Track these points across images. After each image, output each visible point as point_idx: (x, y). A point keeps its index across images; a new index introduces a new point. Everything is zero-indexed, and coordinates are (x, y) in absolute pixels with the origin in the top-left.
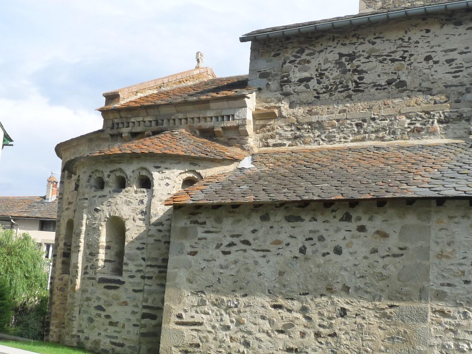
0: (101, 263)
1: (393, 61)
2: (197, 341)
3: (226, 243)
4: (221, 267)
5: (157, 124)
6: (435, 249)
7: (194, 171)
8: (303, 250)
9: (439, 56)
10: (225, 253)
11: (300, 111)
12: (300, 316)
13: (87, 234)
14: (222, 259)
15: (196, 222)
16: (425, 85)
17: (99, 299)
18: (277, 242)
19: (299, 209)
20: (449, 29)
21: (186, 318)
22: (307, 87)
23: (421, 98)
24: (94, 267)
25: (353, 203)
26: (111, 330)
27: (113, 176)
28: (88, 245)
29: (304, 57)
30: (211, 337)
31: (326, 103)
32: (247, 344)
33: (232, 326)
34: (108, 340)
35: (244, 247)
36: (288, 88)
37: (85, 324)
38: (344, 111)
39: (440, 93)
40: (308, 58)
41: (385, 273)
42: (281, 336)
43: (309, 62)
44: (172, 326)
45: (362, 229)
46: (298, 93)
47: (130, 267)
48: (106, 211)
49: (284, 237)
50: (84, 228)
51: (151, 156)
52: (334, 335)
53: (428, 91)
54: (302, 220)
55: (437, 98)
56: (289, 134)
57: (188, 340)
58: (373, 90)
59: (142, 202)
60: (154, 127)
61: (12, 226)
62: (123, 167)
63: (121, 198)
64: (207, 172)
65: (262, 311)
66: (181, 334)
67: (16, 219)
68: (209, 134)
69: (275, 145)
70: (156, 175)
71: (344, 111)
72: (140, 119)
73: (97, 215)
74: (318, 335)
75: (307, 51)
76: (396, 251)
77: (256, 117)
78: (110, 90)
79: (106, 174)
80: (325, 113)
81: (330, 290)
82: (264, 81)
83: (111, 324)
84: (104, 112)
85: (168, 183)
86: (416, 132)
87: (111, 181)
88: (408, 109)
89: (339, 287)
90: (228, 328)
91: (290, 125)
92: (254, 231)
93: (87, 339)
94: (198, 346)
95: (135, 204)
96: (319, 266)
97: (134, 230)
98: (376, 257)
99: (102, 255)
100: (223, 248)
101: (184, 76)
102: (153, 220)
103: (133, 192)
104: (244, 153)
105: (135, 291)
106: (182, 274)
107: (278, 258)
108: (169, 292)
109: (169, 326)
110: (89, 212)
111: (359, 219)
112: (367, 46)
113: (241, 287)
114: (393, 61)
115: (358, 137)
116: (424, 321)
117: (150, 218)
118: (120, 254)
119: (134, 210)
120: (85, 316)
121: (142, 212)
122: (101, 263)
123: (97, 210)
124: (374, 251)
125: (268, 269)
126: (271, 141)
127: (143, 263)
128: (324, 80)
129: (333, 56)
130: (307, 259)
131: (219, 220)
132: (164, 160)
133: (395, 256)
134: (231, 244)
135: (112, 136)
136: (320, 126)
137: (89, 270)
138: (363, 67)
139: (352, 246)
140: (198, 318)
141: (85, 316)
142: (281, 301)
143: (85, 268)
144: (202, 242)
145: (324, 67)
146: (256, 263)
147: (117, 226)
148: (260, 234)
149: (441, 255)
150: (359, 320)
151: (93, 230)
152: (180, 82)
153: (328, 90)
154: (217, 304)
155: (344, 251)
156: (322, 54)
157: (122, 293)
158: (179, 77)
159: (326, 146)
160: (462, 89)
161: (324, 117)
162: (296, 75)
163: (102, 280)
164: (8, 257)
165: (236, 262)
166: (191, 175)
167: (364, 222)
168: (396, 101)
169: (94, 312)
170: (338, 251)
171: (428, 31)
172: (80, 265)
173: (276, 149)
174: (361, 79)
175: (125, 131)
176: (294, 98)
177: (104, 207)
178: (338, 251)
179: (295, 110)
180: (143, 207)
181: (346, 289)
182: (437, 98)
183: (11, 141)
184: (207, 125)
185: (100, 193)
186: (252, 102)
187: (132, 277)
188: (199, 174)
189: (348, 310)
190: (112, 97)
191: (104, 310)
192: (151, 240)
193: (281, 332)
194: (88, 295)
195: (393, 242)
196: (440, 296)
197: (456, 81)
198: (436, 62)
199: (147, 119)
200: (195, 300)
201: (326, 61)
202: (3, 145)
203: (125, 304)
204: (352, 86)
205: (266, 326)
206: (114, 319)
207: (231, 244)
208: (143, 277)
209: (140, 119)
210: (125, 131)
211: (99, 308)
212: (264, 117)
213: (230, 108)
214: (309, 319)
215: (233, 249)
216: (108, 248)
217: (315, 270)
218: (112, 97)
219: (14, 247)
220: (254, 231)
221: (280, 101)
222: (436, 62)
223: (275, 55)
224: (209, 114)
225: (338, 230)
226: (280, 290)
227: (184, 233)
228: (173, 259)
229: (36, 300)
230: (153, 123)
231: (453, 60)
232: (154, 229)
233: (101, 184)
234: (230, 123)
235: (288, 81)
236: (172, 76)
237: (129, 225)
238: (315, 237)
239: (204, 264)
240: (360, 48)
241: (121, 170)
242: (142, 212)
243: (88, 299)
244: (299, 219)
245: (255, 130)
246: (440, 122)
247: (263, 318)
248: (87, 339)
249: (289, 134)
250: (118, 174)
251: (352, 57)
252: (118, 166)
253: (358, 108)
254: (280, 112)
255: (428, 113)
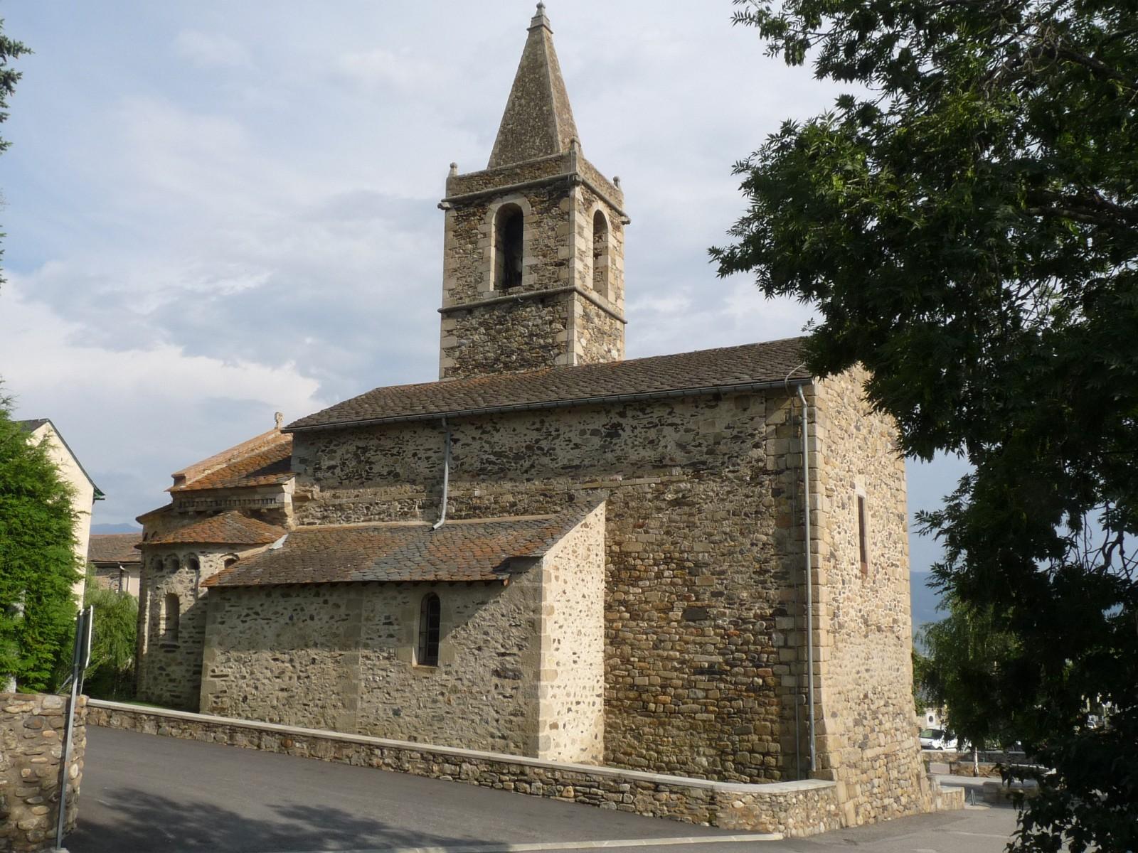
0: (162, 632)
1: (392, 455)
2: (225, 688)
3: (244, 614)
4: (241, 632)
5: (217, 504)
6: (365, 614)
7: (232, 554)
8: (291, 618)
9: (422, 454)
10: (244, 622)
11: (328, 494)
12: (289, 665)
13: (151, 608)
14: (241, 627)
15: (224, 599)
16: (412, 476)
17: (160, 661)
18: (276, 613)
19: (288, 590)
20: (427, 432)
21: (218, 672)
22: (333, 473)
23: (408, 487)
24: (157, 635)
25: (319, 585)
26: (171, 685)
27: (169, 560)
28: (152, 618)
29: (332, 447)
30: (234, 684)
31: (346, 488)
32: (256, 688)
33: (247, 676)
34: (168, 694)
35: (255, 616)
36: (319, 475)
37: (151, 682)
38: (358, 496)
39: (421, 483)
40: (335, 448)
41: (337, 632)
42: (278, 680)
43: (335, 452)
44: (209, 679)
45: (326, 602)
46: (326, 479)
47: (185, 634)
48: (165, 589)
49: (280, 609)
50: (148, 603)
51: (196, 544)
52: (308, 677)
53: (413, 482)
54: (290, 596)
55: (418, 488)
56: (319, 515)
57: (219, 688)
58: (378, 479)
59: (191, 581)
60: (215, 508)
61: (122, 574)
62: (177, 552)
63: (175, 578)
64: (242, 555)
65: (265, 663)
66: (214, 684)
67: (125, 564)
68: (257, 514)
69: (309, 524)
70: (202, 559)
71: (358, 496)
72: (203, 499)
73: (158, 592)
74: (299, 678)
75: (335, 443)
76: (344, 617)
77: (295, 499)
78: (177, 471)
79: (164, 558)
80: (346, 496)
81: (307, 646)
82: (303, 466)
83: (171, 680)
84: (173, 493)
85: (212, 565)
86: (404, 515)
87: (168, 563)
88: (400, 496)
89: (312, 643)
90: (244, 677)
91: (320, 507)
92: (262, 605)
93: (153, 694)
94: (225, 692)
95: (187, 583)
96: (300, 629)
97: (186, 604)
98: (333, 621)
99: (163, 625)
100: (242, 618)
101: (257, 443)
102: (200, 595)
103: (185, 573)
104: (285, 531)
105: (188, 653)
106: (216, 639)
107: (275, 625)
108: (206, 651)
109: (207, 678)
110: (152, 590)
111: (324, 595)
112: (375, 442)
113: (253, 646)
114: (392, 455)
115: (367, 518)
116: (357, 663)
117: (198, 594)
118: (177, 623)
119: (185, 588)
120: (151, 676)
121: (192, 589)
122: (162, 632)
123: (158, 588)
124: (332, 618)
125: (270, 632)
126: (306, 520)
127: (194, 630)
128: (346, 468)
129: (352, 448)
130: (293, 625)
131: (239, 597)
132: (208, 547)
133: (344, 620)
134: (247, 615)
135: (180, 513)
136: (340, 508)
137: (154, 638)
138: (373, 459)
139: (320, 616)
140: (226, 671)
141: (151, 676)
142: (278, 655)
143: (150, 637)
144: (229, 614)
145: (346, 457)
146: (263, 628)
147: (173, 600)
148: (265, 607)
149: (368, 619)
150: (322, 666)
151: (155, 605)
152: (253, 450)
153: (349, 478)
154: (238, 660)
155: (316, 618)
156: (345, 446)
157: (178, 656)
158: (251, 446)
159: (345, 525)
160: (434, 482)
161: (344, 500)
162: (326, 463)
163: (163, 646)
164: (107, 620)
165: (250, 628)
166: (231, 557)
167: (327, 597)
168: (392, 489)
169: (157, 672)
170: (312, 618)
171: (415, 432)
172: (146, 634)
173: (309, 527)
174: (371, 469)
175: (191, 509)
176: (324, 483)
177: (164, 586)
178: (312, 618)
179: (324, 494)
180: (192, 585)
181: (316, 645)
182: (418, 488)
183: (102, 494)
184: (256, 506)
185: (160, 574)
186: (290, 487)
187: (186, 642)
188: (237, 556)
189: (913, 656)
190: (179, 479)
191: (164, 670)
192: (199, 612)
193: (277, 677)
194: (153, 658)
195: (343, 611)
196: (366, 646)
197: (431, 475)
198: (419, 459)
199: (209, 500)
200: (223, 658)
201: (348, 452)
202: (94, 500)
203: (181, 664)
204: (364, 474)
205: (269, 674)
206: (173, 677)
207: (247, 615)
208: (194, 642)
209: (203, 499)
210: (191, 509)
211: (161, 668)
212: (299, 499)
213: (272, 493)
214: (294, 667)
215: (248, 619)
216: (167, 619)
217: (298, 632)
218: (179, 479)
219: (113, 608)
220: (262, 605)
221: (312, 485)
222: (419, 459)
223: (313, 444)
224: (257, 497)
225: (312, 603)
226: (277, 646)
227: (217, 607)
228: (209, 628)
229: (766, 710)
230: (214, 504)
231: (430, 457)
232: (200, 603)
233: (161, 567)
234: (272, 506)
235: (319, 469)
236: (242, 445)
237: (182, 600)
238: (298, 608)
239: (230, 631)
240: (371, 443)
241: (175, 555)
242: (192, 589)
243: (153, 662)
244: (289, 595)
245: (294, 510)
246: (419, 507)
247: (267, 668)
248: (153, 694)
249: (319, 515)
250: (174, 558)
251: (365, 450)
252: (173, 551)
253: (368, 493)
254: (312, 495)
255: (412, 500)
